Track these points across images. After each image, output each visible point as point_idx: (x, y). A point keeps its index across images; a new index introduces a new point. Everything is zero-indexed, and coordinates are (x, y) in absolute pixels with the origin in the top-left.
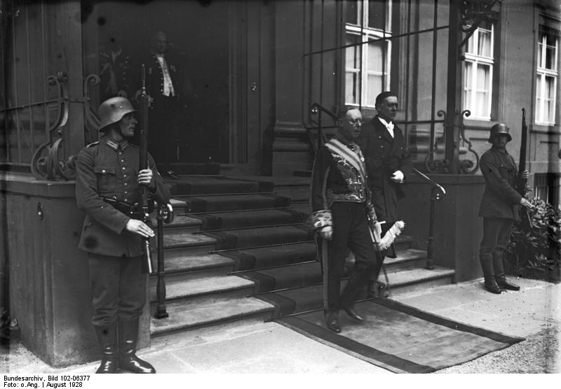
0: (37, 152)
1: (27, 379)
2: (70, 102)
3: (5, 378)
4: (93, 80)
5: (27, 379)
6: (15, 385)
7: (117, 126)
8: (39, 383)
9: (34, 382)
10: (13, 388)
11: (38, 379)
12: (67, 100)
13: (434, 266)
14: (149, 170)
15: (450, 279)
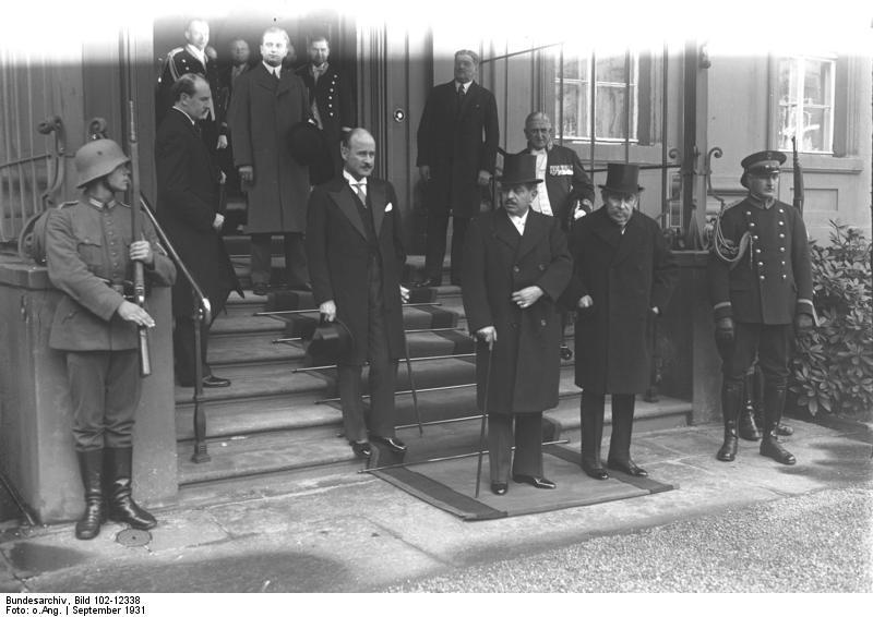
0: (29, 221)
1: (43, 602)
2: (66, 157)
3: (8, 600)
4: (96, 126)
5: (43, 602)
6: (23, 611)
7: (104, 180)
8: (61, 608)
9: (53, 606)
10: (93, 615)
11: (58, 602)
12: (61, 155)
13: (658, 397)
14: (144, 242)
15: (683, 418)
